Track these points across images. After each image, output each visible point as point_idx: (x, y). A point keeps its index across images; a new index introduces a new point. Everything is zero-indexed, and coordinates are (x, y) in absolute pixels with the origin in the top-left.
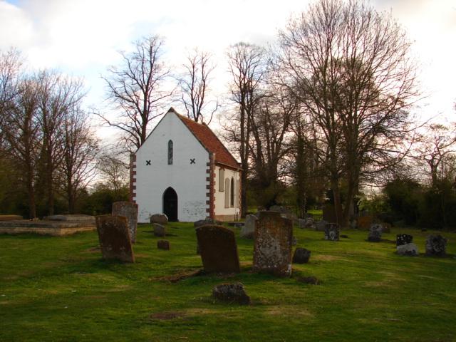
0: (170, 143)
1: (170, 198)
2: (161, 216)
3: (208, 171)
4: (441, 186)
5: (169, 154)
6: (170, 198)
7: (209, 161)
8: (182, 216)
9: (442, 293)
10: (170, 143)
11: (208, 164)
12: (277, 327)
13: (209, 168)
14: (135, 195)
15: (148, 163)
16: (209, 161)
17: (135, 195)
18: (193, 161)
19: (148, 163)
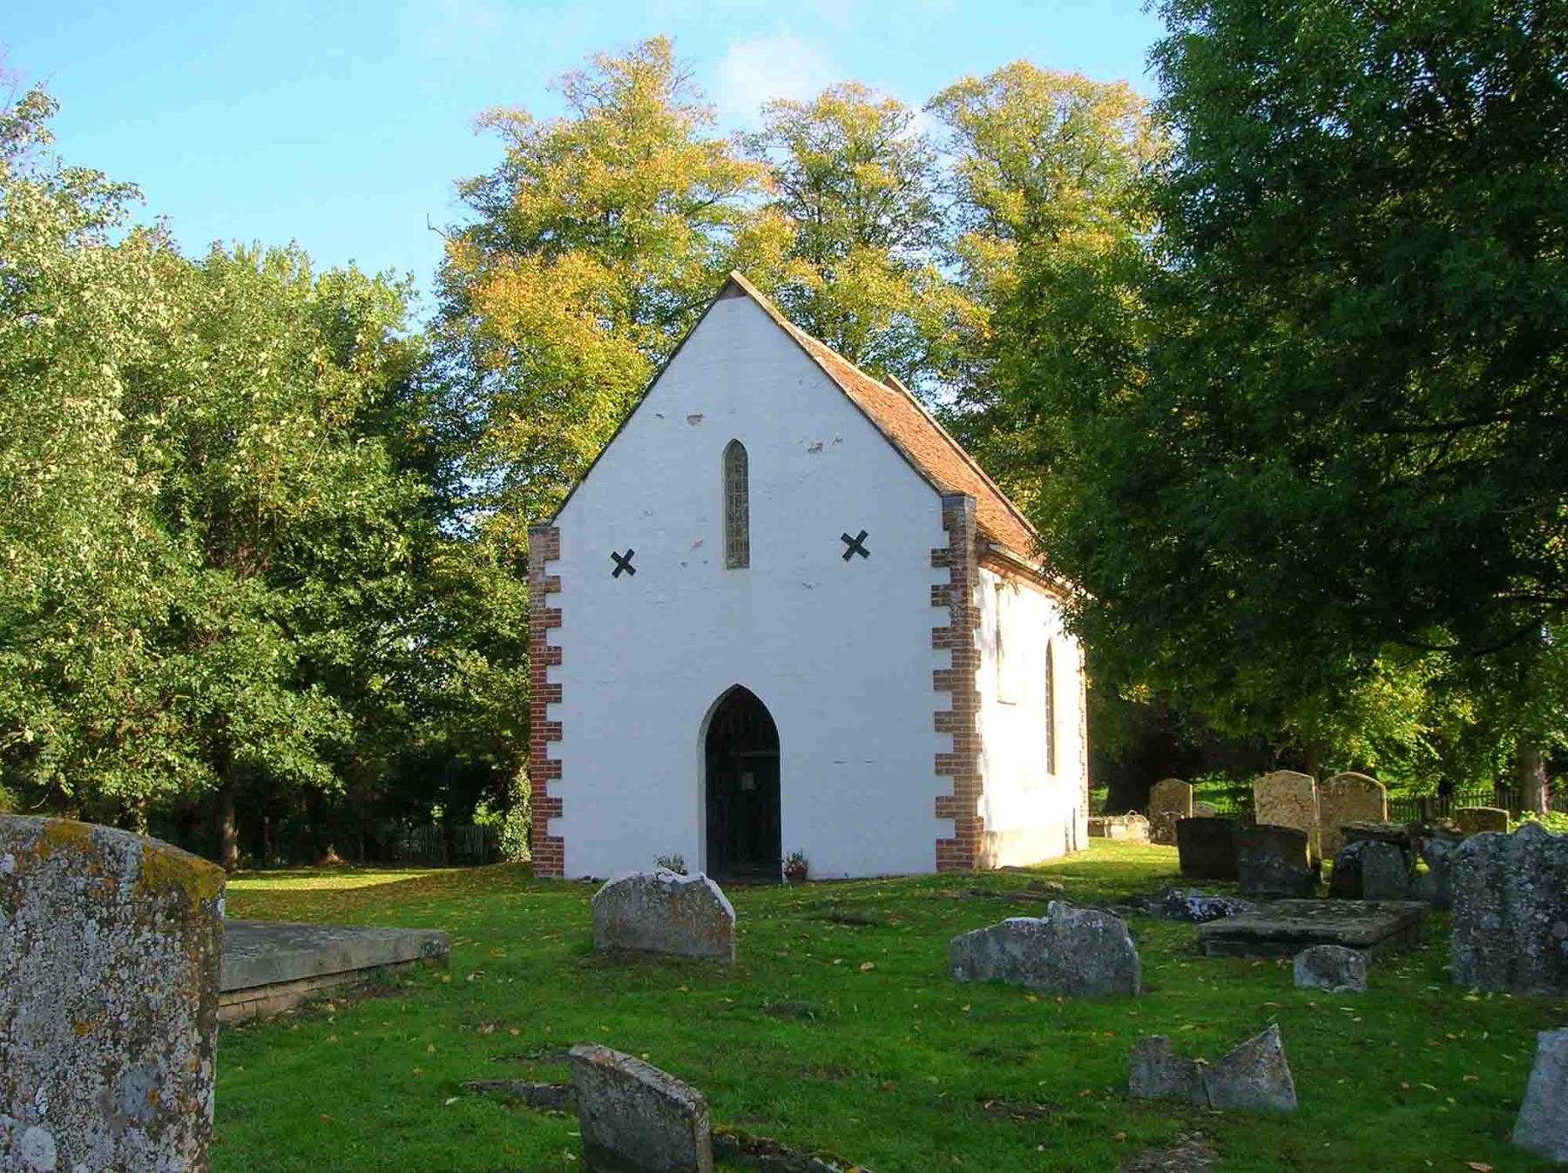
0: (736, 455)
1: (740, 742)
2: (677, 894)
3: (939, 596)
4: (1566, 836)
5: (730, 518)
6: (740, 742)
7: (942, 541)
8: (804, 830)
9: (1084, 1116)
10: (736, 455)
11: (939, 559)
12: (302, 988)
13: (943, 577)
14: (555, 694)
15: (623, 564)
16: (942, 541)
17: (556, 731)
18: (855, 546)
19: (623, 564)
